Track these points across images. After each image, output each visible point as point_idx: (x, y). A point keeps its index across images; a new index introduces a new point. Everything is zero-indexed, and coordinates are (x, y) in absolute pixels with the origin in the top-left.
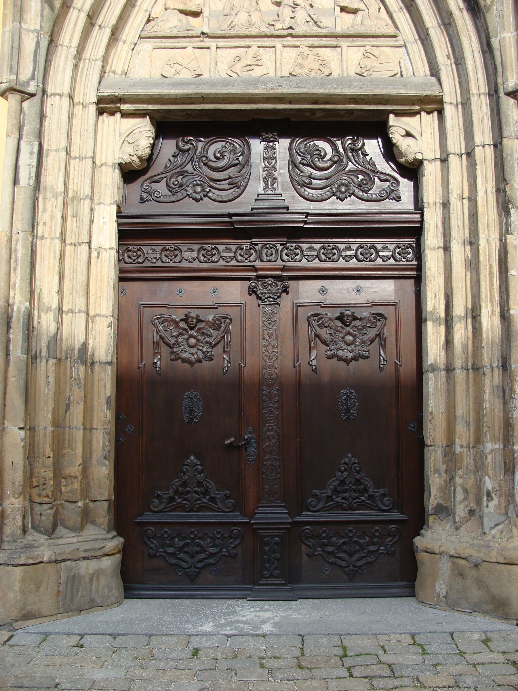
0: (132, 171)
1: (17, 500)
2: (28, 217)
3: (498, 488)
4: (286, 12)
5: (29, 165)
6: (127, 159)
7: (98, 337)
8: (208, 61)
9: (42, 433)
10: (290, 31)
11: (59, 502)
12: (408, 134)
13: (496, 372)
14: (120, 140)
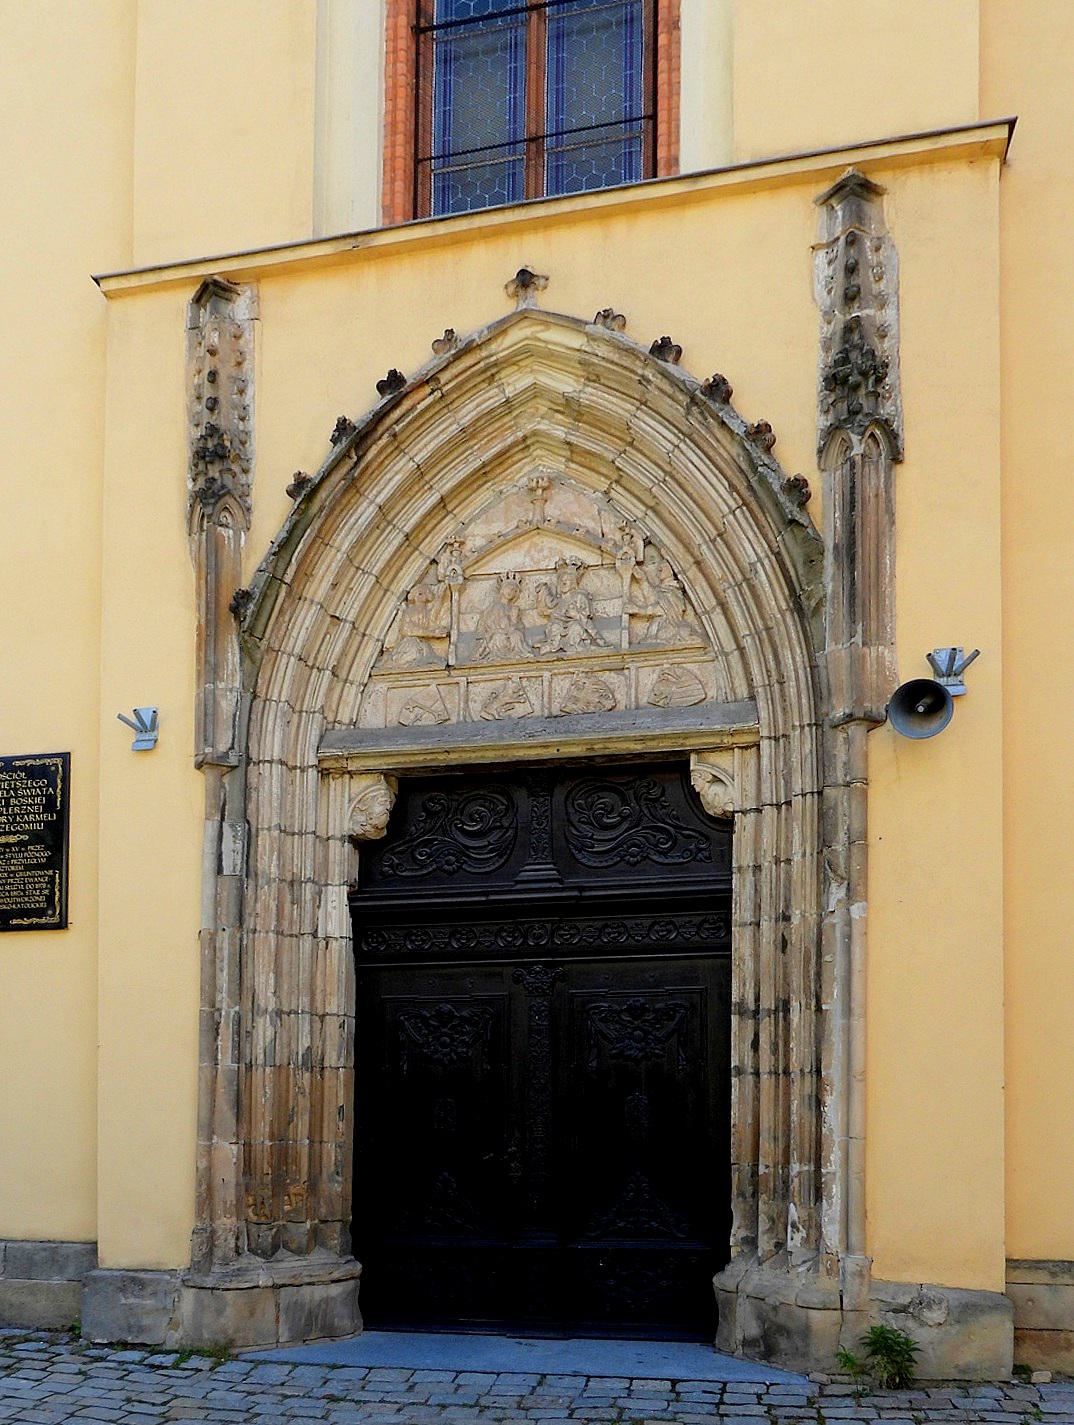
1: (229, 1221)
2: (234, 910)
3: (806, 1218)
6: (359, 830)
7: (327, 1039)
9: (259, 1148)
10: (560, 655)
11: (281, 1223)
12: (716, 780)
13: (808, 1078)
14: (349, 807)
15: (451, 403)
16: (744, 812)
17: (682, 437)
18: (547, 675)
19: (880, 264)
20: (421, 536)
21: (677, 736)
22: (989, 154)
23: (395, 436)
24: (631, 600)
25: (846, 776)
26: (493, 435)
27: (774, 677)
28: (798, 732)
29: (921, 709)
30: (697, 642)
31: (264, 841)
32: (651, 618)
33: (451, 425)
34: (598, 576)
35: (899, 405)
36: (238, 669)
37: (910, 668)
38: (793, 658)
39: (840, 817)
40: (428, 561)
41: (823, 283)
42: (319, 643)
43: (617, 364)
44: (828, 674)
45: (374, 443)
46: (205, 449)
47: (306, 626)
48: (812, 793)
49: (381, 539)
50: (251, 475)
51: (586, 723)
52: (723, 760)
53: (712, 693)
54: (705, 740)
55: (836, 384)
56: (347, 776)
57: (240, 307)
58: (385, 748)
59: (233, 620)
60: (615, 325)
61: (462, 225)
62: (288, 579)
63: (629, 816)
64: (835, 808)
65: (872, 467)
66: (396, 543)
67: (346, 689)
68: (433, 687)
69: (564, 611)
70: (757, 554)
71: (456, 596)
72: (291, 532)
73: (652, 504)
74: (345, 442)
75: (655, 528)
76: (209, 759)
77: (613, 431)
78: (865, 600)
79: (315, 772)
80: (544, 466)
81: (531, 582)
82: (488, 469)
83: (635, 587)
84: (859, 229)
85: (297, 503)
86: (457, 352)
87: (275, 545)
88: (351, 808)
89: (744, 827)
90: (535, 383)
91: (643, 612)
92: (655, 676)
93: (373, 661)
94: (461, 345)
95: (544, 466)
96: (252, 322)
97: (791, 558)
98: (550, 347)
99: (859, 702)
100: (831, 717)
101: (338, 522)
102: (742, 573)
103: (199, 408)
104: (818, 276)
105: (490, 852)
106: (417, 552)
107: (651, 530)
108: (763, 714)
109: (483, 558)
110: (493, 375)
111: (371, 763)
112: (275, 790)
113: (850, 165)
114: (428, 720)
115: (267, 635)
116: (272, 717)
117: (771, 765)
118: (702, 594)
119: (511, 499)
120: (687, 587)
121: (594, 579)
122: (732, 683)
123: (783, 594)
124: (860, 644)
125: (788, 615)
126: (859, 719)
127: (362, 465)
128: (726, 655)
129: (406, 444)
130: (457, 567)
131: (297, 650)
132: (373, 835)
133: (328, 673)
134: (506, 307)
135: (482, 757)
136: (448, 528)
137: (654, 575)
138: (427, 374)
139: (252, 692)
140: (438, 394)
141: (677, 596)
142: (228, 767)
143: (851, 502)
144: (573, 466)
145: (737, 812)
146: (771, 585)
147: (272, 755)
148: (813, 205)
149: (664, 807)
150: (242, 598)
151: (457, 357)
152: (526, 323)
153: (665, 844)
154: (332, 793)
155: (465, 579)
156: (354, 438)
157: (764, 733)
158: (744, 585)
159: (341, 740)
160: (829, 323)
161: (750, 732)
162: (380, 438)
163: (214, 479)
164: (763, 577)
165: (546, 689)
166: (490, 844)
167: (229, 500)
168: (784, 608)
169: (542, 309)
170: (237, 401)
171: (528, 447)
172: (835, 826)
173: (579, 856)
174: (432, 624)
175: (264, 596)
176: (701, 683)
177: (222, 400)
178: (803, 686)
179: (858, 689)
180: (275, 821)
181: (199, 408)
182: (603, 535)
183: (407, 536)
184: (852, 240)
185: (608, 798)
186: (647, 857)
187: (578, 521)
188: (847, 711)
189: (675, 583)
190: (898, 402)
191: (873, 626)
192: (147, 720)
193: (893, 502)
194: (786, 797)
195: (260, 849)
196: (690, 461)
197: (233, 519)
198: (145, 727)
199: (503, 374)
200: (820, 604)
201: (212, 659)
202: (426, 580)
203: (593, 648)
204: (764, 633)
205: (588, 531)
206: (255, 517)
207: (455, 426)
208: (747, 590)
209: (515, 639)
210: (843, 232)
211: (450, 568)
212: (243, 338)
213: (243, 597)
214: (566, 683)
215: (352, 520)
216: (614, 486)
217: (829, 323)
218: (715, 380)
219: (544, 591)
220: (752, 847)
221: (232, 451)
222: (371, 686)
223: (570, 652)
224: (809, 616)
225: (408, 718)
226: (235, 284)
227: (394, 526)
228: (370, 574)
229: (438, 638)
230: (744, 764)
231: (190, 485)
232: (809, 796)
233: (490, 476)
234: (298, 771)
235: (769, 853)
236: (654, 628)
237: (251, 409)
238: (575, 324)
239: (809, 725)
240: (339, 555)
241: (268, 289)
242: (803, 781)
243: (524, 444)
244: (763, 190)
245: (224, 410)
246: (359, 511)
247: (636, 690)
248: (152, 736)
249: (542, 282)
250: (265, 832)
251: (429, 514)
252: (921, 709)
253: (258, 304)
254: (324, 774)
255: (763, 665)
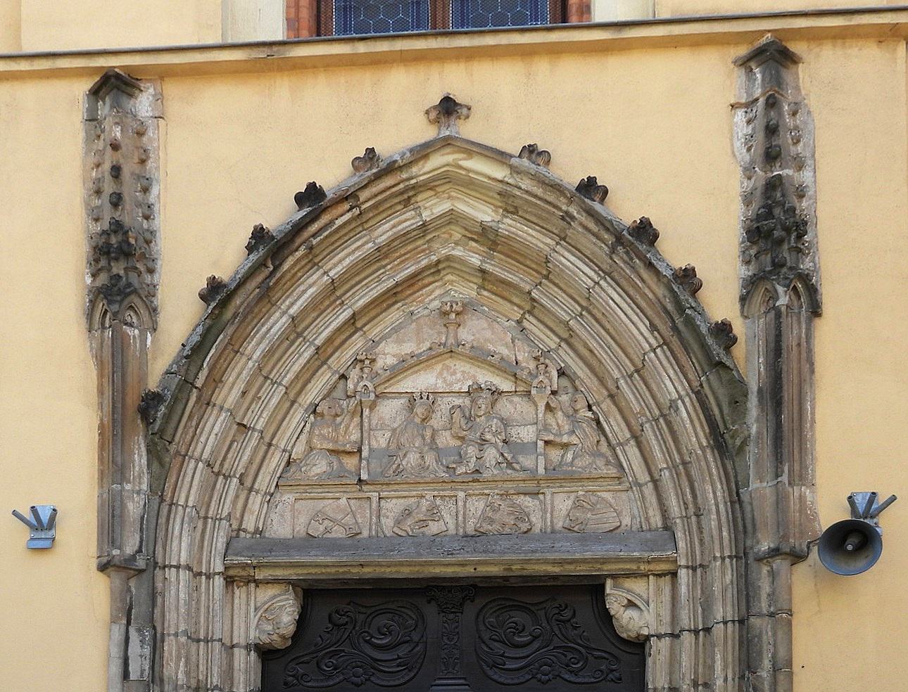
0: (271, 650)
4: (472, 451)
5: (141, 656)
6: (265, 639)
8: (368, 515)
10: (476, 476)
12: (631, 604)
15: (366, 222)
16: (659, 636)
17: (603, 275)
18: (461, 495)
19: (796, 128)
20: (330, 350)
21: (596, 561)
22: (897, 36)
23: (311, 248)
24: (546, 428)
25: (770, 606)
26: (407, 256)
27: (692, 509)
28: (718, 563)
29: (850, 548)
30: (613, 471)
31: (170, 647)
32: (565, 446)
33: (366, 243)
34: (511, 402)
35: (817, 262)
36: (145, 471)
37: (830, 511)
38: (714, 494)
39: (765, 645)
40: (337, 376)
41: (743, 140)
42: (225, 449)
43: (540, 199)
44: (752, 510)
45: (291, 253)
46: (108, 245)
47: (215, 431)
48: (733, 621)
49: (291, 351)
50: (156, 276)
51: (504, 544)
52: (638, 586)
53: (626, 521)
54: (621, 566)
55: (760, 236)
56: (253, 585)
57: (143, 104)
58: (297, 559)
59: (139, 421)
60: (540, 160)
61: (383, 47)
62: (199, 383)
63: (539, 636)
64: (760, 636)
65: (795, 318)
66: (307, 355)
67: (251, 498)
68: (343, 501)
69: (479, 434)
70: (677, 392)
71: (366, 412)
72: (204, 336)
73: (565, 335)
74: (262, 251)
75: (570, 361)
76: (116, 561)
77: (528, 263)
78: (788, 440)
79: (222, 579)
80: (456, 291)
81: (444, 405)
82: (399, 289)
83: (549, 416)
84: (778, 93)
85: (211, 307)
86: (380, 171)
87: (187, 348)
88: (257, 617)
89: (659, 652)
90: (452, 209)
91: (558, 440)
92: (570, 502)
93: (280, 471)
94: (383, 165)
95: (456, 291)
96: (156, 120)
97: (717, 399)
98: (470, 175)
99: (785, 537)
100: (756, 550)
101: (248, 331)
102: (659, 409)
103: (97, 202)
104: (737, 133)
105: (398, 666)
106: (325, 366)
107: (564, 361)
108: (681, 544)
109: (395, 377)
110: (409, 198)
111: (280, 573)
112: (182, 595)
113: (769, 31)
114: (338, 533)
115: (177, 439)
116: (178, 521)
117: (689, 592)
118: (616, 427)
119: (422, 321)
120: (601, 419)
121: (508, 405)
122: (647, 513)
123: (704, 431)
124: (787, 482)
125: (708, 451)
126: (786, 554)
127: (278, 275)
128: (640, 485)
129: (320, 257)
130: (369, 384)
131: (205, 456)
132: (279, 644)
133: (235, 480)
134: (428, 133)
135: (396, 572)
136: (357, 344)
137: (567, 404)
138: (348, 190)
139: (160, 494)
140: (356, 211)
141: (592, 427)
142: (134, 570)
143: (776, 350)
144: (485, 293)
145: (653, 636)
146: (692, 421)
147: (179, 560)
148: (732, 66)
149: (575, 628)
150: (153, 399)
151: (378, 177)
152: (448, 150)
153: (575, 664)
154: (236, 601)
155: (376, 396)
156: (269, 248)
157: (683, 562)
158: (661, 420)
159: (249, 548)
160: (749, 178)
161: (667, 560)
162: (297, 250)
163: (118, 277)
164: (684, 414)
165: (461, 509)
166: (399, 658)
167: (135, 300)
168: (705, 444)
169: (463, 137)
170: (140, 199)
171: (439, 271)
172: (760, 653)
173: (490, 673)
174: (341, 438)
175: (175, 399)
176: (615, 511)
177: (126, 197)
178: (723, 519)
179: (782, 522)
180: (182, 628)
181: (97, 202)
182: (517, 363)
183: (318, 349)
184: (772, 103)
185: (519, 617)
186: (558, 676)
187: (491, 348)
188: (772, 546)
189: (590, 414)
190: (817, 258)
191: (797, 467)
192: (45, 517)
193: (813, 353)
194: (703, 624)
195: (166, 654)
196: (611, 298)
197: (139, 319)
198: (42, 527)
199: (419, 198)
200: (745, 443)
201: (119, 459)
202: (334, 394)
203: (509, 471)
204: (681, 467)
205: (502, 359)
206: (162, 319)
207: (370, 245)
208: (664, 426)
209: (430, 459)
210: (763, 94)
211: (361, 384)
212: (146, 136)
213: (150, 402)
214: (481, 505)
215: (264, 329)
216: (527, 316)
217: (749, 178)
218: (641, 221)
219: (457, 415)
220: (667, 671)
221: (137, 248)
222: (278, 496)
223: (486, 475)
224: (734, 454)
225: (318, 529)
226: (137, 79)
227: (304, 339)
228: (280, 384)
229: (349, 453)
230: (658, 590)
231: (89, 280)
232: (730, 625)
233: (400, 297)
234: (204, 577)
235: (688, 676)
236: (569, 456)
237: (156, 208)
238: (499, 156)
239: (730, 557)
240: (250, 364)
241: (172, 89)
242: (723, 610)
243: (436, 269)
244: (683, 45)
245: (127, 207)
246: (271, 321)
247: (552, 515)
248: (50, 534)
249: (465, 111)
250: (172, 637)
251: (339, 330)
252: (850, 548)
253: (162, 102)
254: (230, 581)
255: (681, 497)
